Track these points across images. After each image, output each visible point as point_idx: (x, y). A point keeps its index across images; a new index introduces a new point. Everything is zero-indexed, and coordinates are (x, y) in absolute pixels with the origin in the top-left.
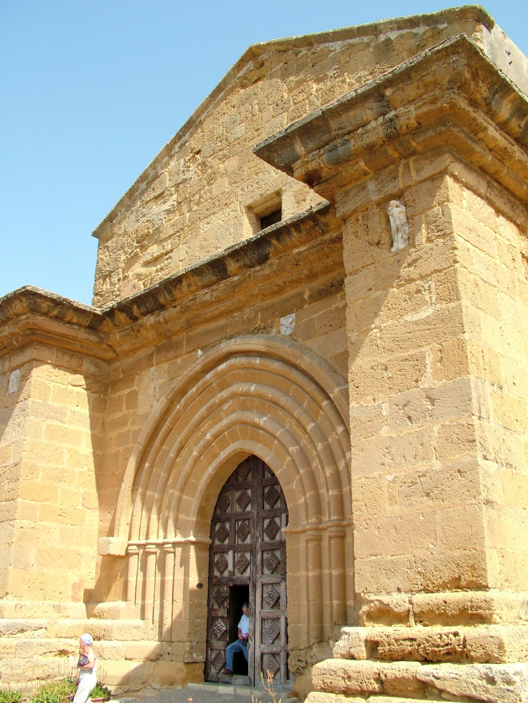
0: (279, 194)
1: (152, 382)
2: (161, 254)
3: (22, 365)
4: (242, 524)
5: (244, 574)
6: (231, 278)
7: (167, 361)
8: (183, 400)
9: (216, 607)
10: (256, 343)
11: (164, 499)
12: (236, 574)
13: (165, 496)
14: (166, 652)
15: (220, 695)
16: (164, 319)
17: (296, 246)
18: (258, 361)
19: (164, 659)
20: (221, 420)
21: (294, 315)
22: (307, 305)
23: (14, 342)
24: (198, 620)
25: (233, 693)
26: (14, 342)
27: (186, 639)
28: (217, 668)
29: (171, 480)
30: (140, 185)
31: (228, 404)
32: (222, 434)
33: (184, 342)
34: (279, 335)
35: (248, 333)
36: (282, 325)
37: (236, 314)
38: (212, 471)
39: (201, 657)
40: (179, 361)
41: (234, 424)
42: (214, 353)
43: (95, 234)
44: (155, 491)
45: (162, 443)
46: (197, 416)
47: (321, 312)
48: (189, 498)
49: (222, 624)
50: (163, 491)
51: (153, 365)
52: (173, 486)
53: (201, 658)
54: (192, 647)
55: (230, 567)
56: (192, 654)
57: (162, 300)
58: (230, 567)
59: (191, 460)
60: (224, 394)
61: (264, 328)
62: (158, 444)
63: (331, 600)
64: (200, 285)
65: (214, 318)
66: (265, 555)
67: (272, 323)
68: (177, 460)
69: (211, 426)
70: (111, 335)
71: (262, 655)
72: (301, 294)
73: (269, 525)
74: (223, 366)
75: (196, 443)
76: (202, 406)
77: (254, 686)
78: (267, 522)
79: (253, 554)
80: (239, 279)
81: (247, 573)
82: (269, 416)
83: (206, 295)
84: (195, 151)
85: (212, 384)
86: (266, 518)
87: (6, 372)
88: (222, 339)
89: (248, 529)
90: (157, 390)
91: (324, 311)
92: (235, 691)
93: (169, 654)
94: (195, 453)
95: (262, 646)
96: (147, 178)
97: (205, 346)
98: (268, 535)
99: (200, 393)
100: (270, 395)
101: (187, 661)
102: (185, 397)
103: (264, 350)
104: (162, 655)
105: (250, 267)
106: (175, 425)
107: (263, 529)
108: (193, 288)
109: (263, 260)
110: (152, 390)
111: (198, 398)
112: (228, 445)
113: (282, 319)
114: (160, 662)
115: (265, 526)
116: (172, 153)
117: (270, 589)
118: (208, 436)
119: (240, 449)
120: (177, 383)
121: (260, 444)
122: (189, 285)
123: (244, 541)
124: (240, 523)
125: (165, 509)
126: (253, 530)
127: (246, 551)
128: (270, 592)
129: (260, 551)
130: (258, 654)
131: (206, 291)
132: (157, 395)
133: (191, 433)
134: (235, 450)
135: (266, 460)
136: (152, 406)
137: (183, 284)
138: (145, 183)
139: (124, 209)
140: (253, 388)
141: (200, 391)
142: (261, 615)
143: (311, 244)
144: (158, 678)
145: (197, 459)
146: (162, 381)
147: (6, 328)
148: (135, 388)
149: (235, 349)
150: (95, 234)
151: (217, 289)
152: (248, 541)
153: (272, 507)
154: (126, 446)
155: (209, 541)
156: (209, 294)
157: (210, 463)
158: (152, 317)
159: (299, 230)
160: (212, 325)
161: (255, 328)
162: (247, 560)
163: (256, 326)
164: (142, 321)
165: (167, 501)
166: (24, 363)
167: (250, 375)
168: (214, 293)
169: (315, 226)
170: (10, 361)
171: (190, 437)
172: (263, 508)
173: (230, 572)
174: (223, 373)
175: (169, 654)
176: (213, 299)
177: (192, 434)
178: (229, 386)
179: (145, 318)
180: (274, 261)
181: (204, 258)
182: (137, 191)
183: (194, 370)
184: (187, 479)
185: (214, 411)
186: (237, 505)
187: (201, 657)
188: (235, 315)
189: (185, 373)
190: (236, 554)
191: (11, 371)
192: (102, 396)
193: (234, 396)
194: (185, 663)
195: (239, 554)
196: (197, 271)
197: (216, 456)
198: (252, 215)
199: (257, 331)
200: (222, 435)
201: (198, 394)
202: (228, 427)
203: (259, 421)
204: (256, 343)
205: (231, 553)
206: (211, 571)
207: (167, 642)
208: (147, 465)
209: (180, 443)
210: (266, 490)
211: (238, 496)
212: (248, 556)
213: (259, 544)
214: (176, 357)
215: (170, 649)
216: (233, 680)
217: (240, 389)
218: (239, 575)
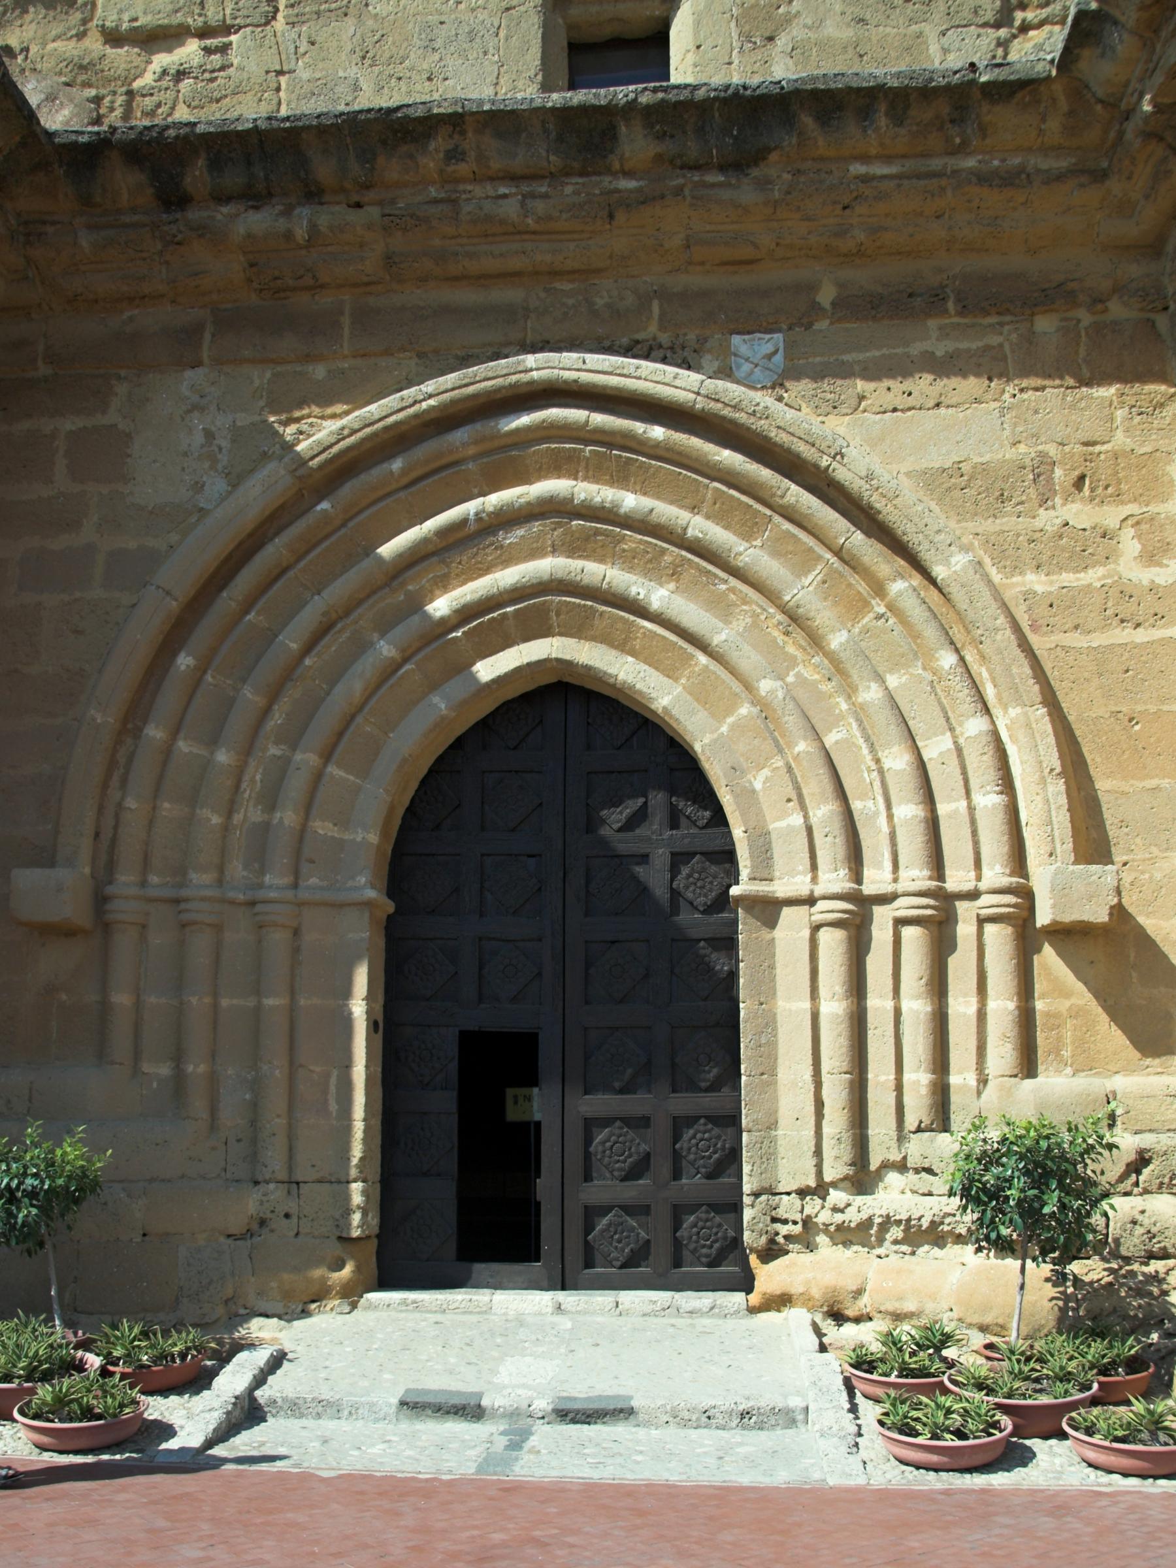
1: (196, 414)
2: (180, 25)
14: (281, 1209)
16: (313, 228)
17: (865, 158)
21: (778, 337)
22: (827, 322)
29: (277, 718)
33: (346, 321)
44: (213, 741)
45: (248, 605)
47: (877, 353)
48: (351, 778)
51: (197, 364)
63: (213, 1079)
65: (484, 279)
68: (308, 662)
72: (812, 288)
80: (639, 190)
88: (508, 344)
91: (885, 351)
94: (386, 649)
108: (463, 169)
113: (736, 340)
125: (251, 804)
131: (503, 190)
141: (414, 475)
143: (909, 165)
145: (391, 669)
151: (545, 196)
154: (78, 594)
159: (898, 120)
160: (467, 296)
164: (205, 214)
165: (258, 777)
168: (540, 206)
169: (952, 121)
175: (287, 1216)
176: (530, 221)
177: (368, 597)
179: (225, 210)
188: (558, 285)
201: (405, 481)
208: (184, 661)
214: (309, 358)
215: (292, 1206)
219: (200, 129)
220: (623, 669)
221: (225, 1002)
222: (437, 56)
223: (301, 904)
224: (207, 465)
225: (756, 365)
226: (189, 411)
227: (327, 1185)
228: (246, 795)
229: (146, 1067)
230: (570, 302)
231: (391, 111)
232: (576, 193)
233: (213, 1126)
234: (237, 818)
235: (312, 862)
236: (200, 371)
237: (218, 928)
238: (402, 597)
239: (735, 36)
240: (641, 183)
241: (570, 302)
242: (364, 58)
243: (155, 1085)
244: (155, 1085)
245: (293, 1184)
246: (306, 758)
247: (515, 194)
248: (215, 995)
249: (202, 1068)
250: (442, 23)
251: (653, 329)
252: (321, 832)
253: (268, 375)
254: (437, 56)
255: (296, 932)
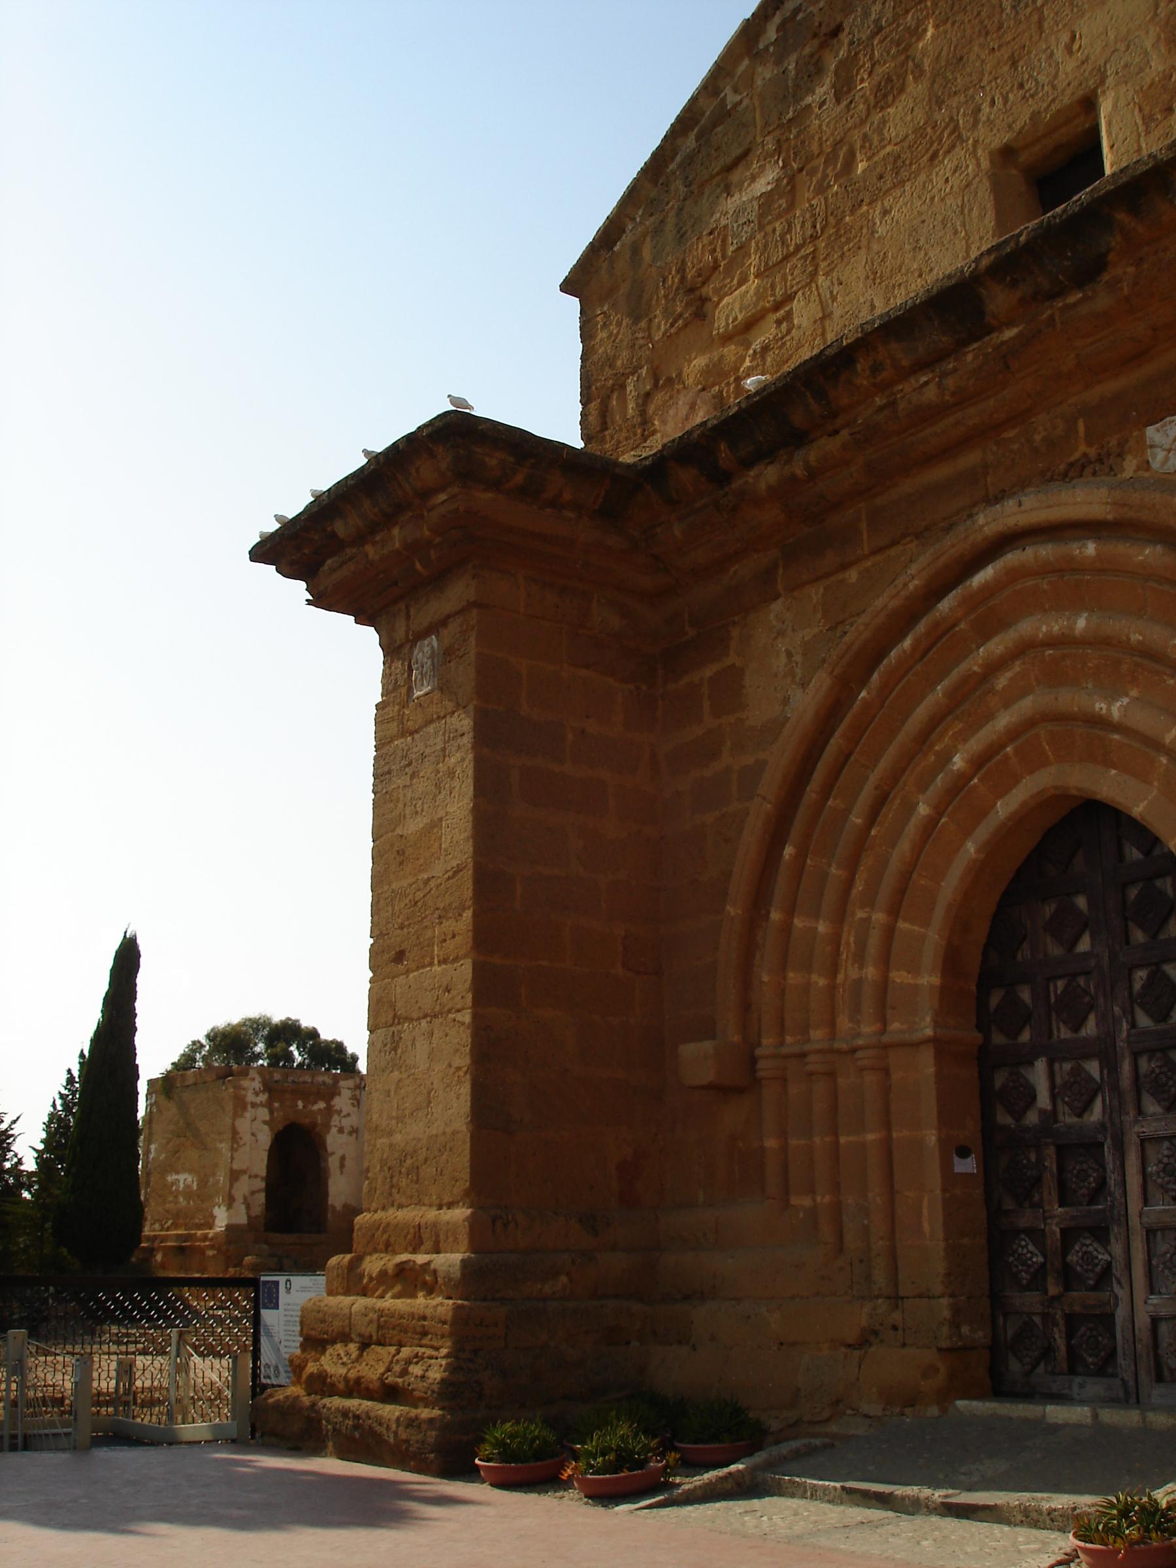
0: (1089, 104)
1: (780, 639)
3: (444, 622)
4: (1066, 987)
5: (1086, 1116)
6: (994, 335)
7: (818, 579)
8: (876, 676)
9: (1009, 1204)
10: (1084, 500)
11: (845, 935)
12: (1061, 1117)
13: (846, 929)
15: (1055, 1428)
18: (1091, 548)
19: (882, 1341)
20: (991, 716)
23: (418, 566)
24: (966, 1241)
25: (1089, 1420)
26: (418, 566)
27: (938, 1287)
28: (1027, 1360)
29: (859, 886)
30: (679, 141)
31: (1009, 674)
32: (997, 753)
33: (864, 526)
34: (1147, 474)
35: (1052, 479)
36: (1152, 447)
37: (1011, 433)
38: (978, 851)
39: (980, 1334)
40: (852, 575)
41: (1030, 723)
42: (954, 545)
43: (568, 287)
44: (817, 917)
45: (826, 792)
46: (921, 712)
48: (917, 928)
49: (1031, 1247)
50: (840, 916)
51: (776, 597)
52: (869, 901)
53: (981, 1336)
54: (956, 1310)
55: (1043, 1100)
56: (958, 1327)
57: (797, 418)
58: (1043, 1100)
59: (912, 828)
60: (996, 646)
61: (1100, 460)
62: (814, 795)
64: (905, 363)
66: (1144, 1064)
67: (1121, 445)
68: (873, 833)
69: (963, 737)
70: (659, 530)
71: (1155, 1321)
73: (1149, 983)
74: (985, 575)
75: (923, 787)
76: (932, 685)
77: (1138, 1401)
78: (1141, 975)
79: (1110, 1065)
80: (1020, 334)
81: (1096, 1113)
82: (1134, 693)
83: (925, 389)
84: (824, 30)
85: (955, 625)
86: (1140, 966)
87: (401, 646)
88: (975, 504)
89: (1086, 999)
90: (798, 658)
92: (1095, 1416)
93: (895, 1328)
94: (923, 810)
95: (1154, 1299)
96: (697, 123)
97: (927, 529)
98: (1147, 1012)
99: (921, 652)
100: (1136, 637)
101: (945, 1344)
102: (882, 667)
103: (1110, 517)
104: (875, 1333)
105: (1051, 296)
106: (857, 743)
107: (1131, 994)
109: (1088, 272)
110: (783, 659)
111: (918, 667)
112: (1016, 780)
113: (1150, 431)
114: (873, 1349)
115: (1137, 986)
116: (761, 46)
117: (1166, 1152)
118: (958, 762)
119: (1056, 788)
120: (859, 630)
121: (1113, 772)
122: (876, 369)
123: (1076, 1030)
124: (1060, 984)
125: (850, 962)
126: (1101, 1000)
127: (1088, 1057)
128: (1165, 1160)
129: (1127, 1054)
130: (1143, 1320)
131: (924, 379)
132: (798, 671)
133: (908, 758)
134: (1039, 793)
135: (1138, 810)
136: (786, 701)
137: (859, 367)
138: (692, 136)
139: (640, 212)
140: (1081, 623)
142: (1145, 1219)
144: (874, 1390)
145: (930, 825)
146: (807, 634)
147: (396, 531)
148: (732, 659)
149: (1021, 523)
150: (568, 287)
151: (955, 370)
152: (1090, 1028)
153: (1154, 937)
155: (976, 1037)
156: (932, 386)
157: (967, 833)
158: (770, 468)
160: (942, 472)
161: (1071, 465)
162: (1090, 1078)
163: (1072, 459)
164: (741, 481)
165: (852, 939)
166: (449, 616)
167: (1070, 586)
168: (950, 382)
170: (408, 617)
171: (904, 770)
172: (1128, 942)
173: (1042, 1112)
174: (989, 590)
175: (895, 1328)
178: (1003, 625)
179: (752, 473)
180: (1122, 270)
181: (910, 289)
182: (673, 159)
183: (902, 593)
184: (906, 878)
185: (969, 700)
186: (1049, 939)
187: (980, 1334)
188: (1005, 435)
189: (879, 603)
190: (1057, 1066)
191: (413, 643)
192: (644, 688)
193: (1024, 648)
194: (940, 1350)
195: (1067, 1066)
196: (898, 326)
197: (983, 813)
198: (1014, 172)
199: (1075, 471)
200: (998, 757)
202: (1013, 734)
203: (1109, 709)
204: (1084, 500)
205: (1041, 1065)
206: (987, 1115)
207: (888, 1298)
208: (789, 851)
209: (876, 788)
210: (1133, 893)
211: (1048, 916)
212: (1093, 1068)
213: (1124, 1035)
214: (844, 567)
215: (896, 1317)
216: (1076, 1389)
217: (1044, 629)
218: (1071, 1120)
219: (709, 425)
220: (1110, 785)
221: (843, 1140)
222: (923, 253)
223: (886, 1047)
224: (789, 680)
225: (1169, 451)
226: (776, 638)
227: (926, 1300)
228: (844, 957)
229: (795, 1200)
230: (1015, 447)
231: (817, 356)
232: (976, 357)
233: (840, 1249)
234: (841, 977)
235: (893, 1008)
236: (780, 602)
237: (832, 1075)
238: (933, 758)
239: (1139, 122)
240: (1021, 328)
241: (1015, 447)
242: (874, 279)
243: (801, 1215)
244: (801, 1215)
245: (896, 1299)
246: (879, 917)
247: (933, 378)
248: (836, 1135)
249: (827, 1198)
250: (923, 222)
251: (1083, 448)
252: (898, 981)
253: (821, 590)
254: (923, 253)
255: (886, 1072)
